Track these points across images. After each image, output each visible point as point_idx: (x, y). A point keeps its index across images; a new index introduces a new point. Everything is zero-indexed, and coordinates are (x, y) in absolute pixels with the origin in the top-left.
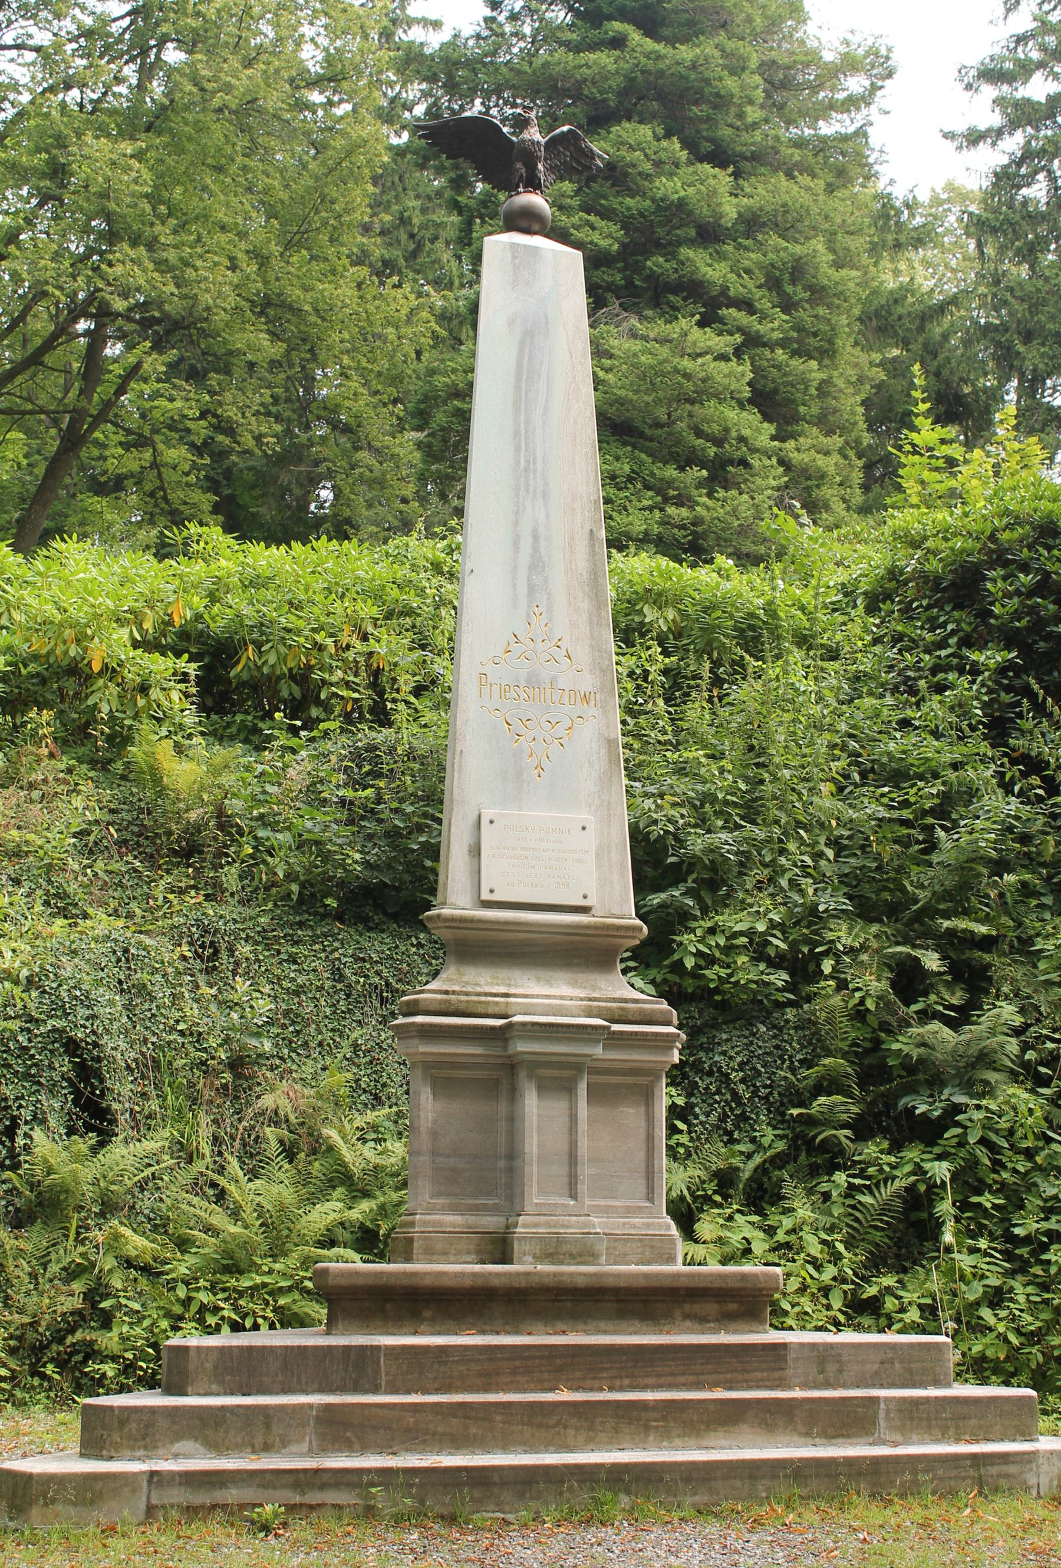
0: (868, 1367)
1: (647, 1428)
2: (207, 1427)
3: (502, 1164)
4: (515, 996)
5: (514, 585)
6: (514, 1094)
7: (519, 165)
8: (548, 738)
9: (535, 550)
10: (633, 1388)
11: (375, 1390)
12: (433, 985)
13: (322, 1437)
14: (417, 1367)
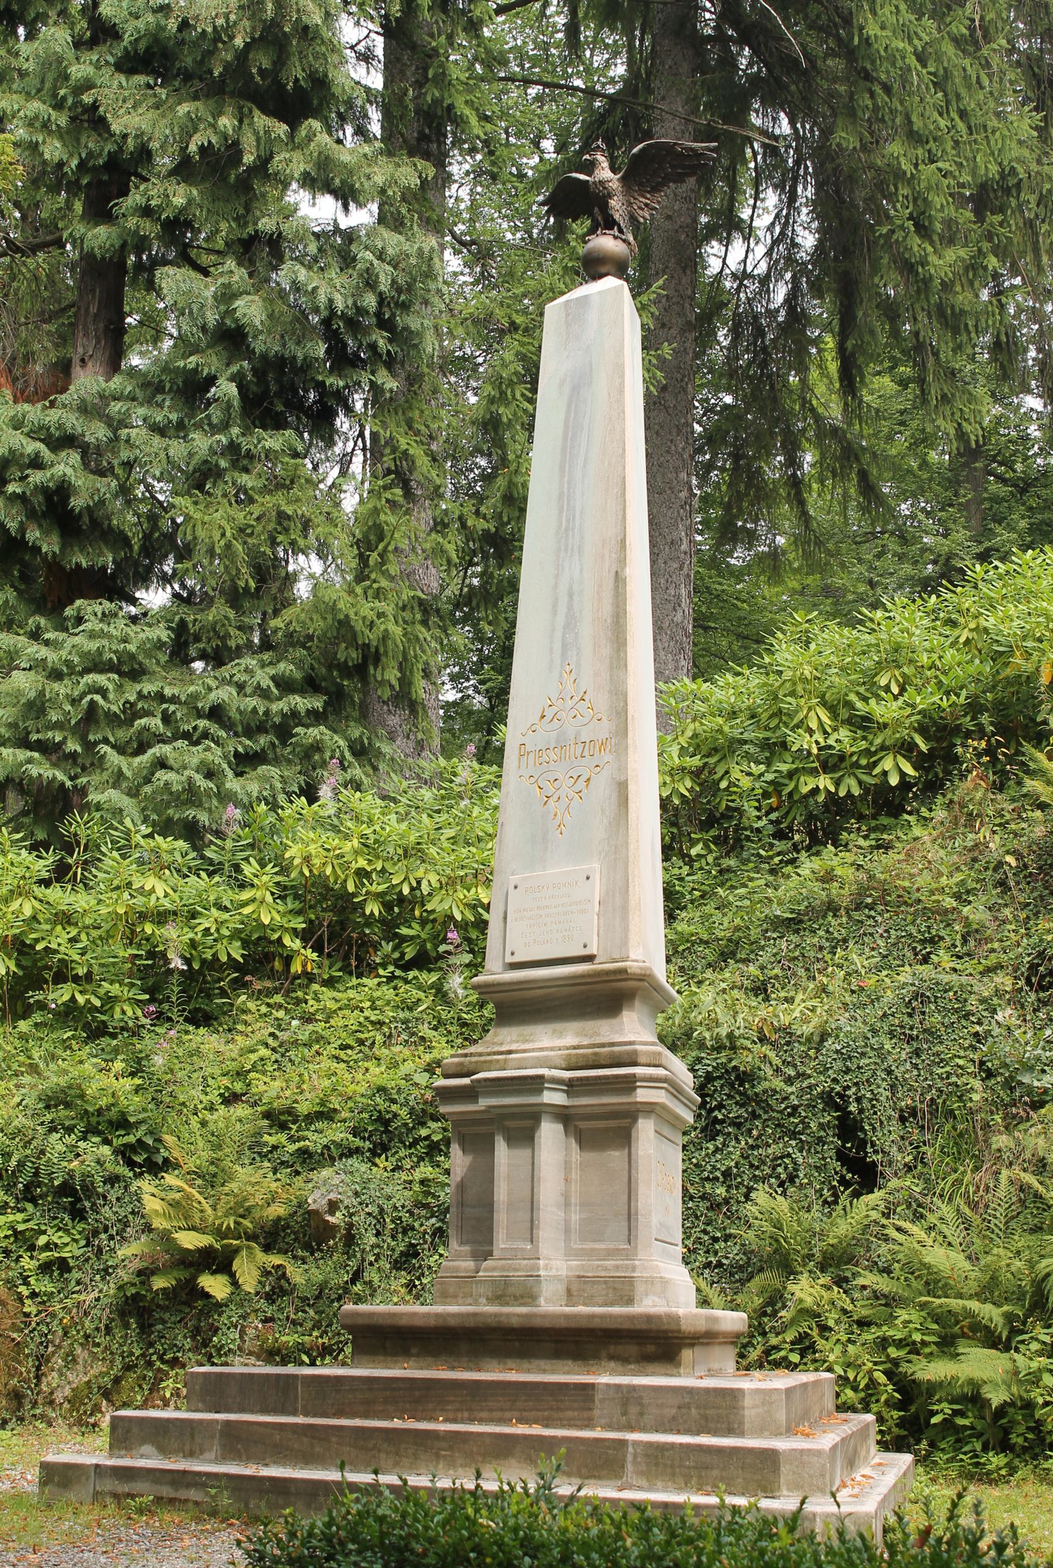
0: (667, 1411)
1: (438, 1456)
4: (510, 1052)
9: (570, 607)
10: (471, 1420)
11: (294, 1413)
13: (223, 1447)
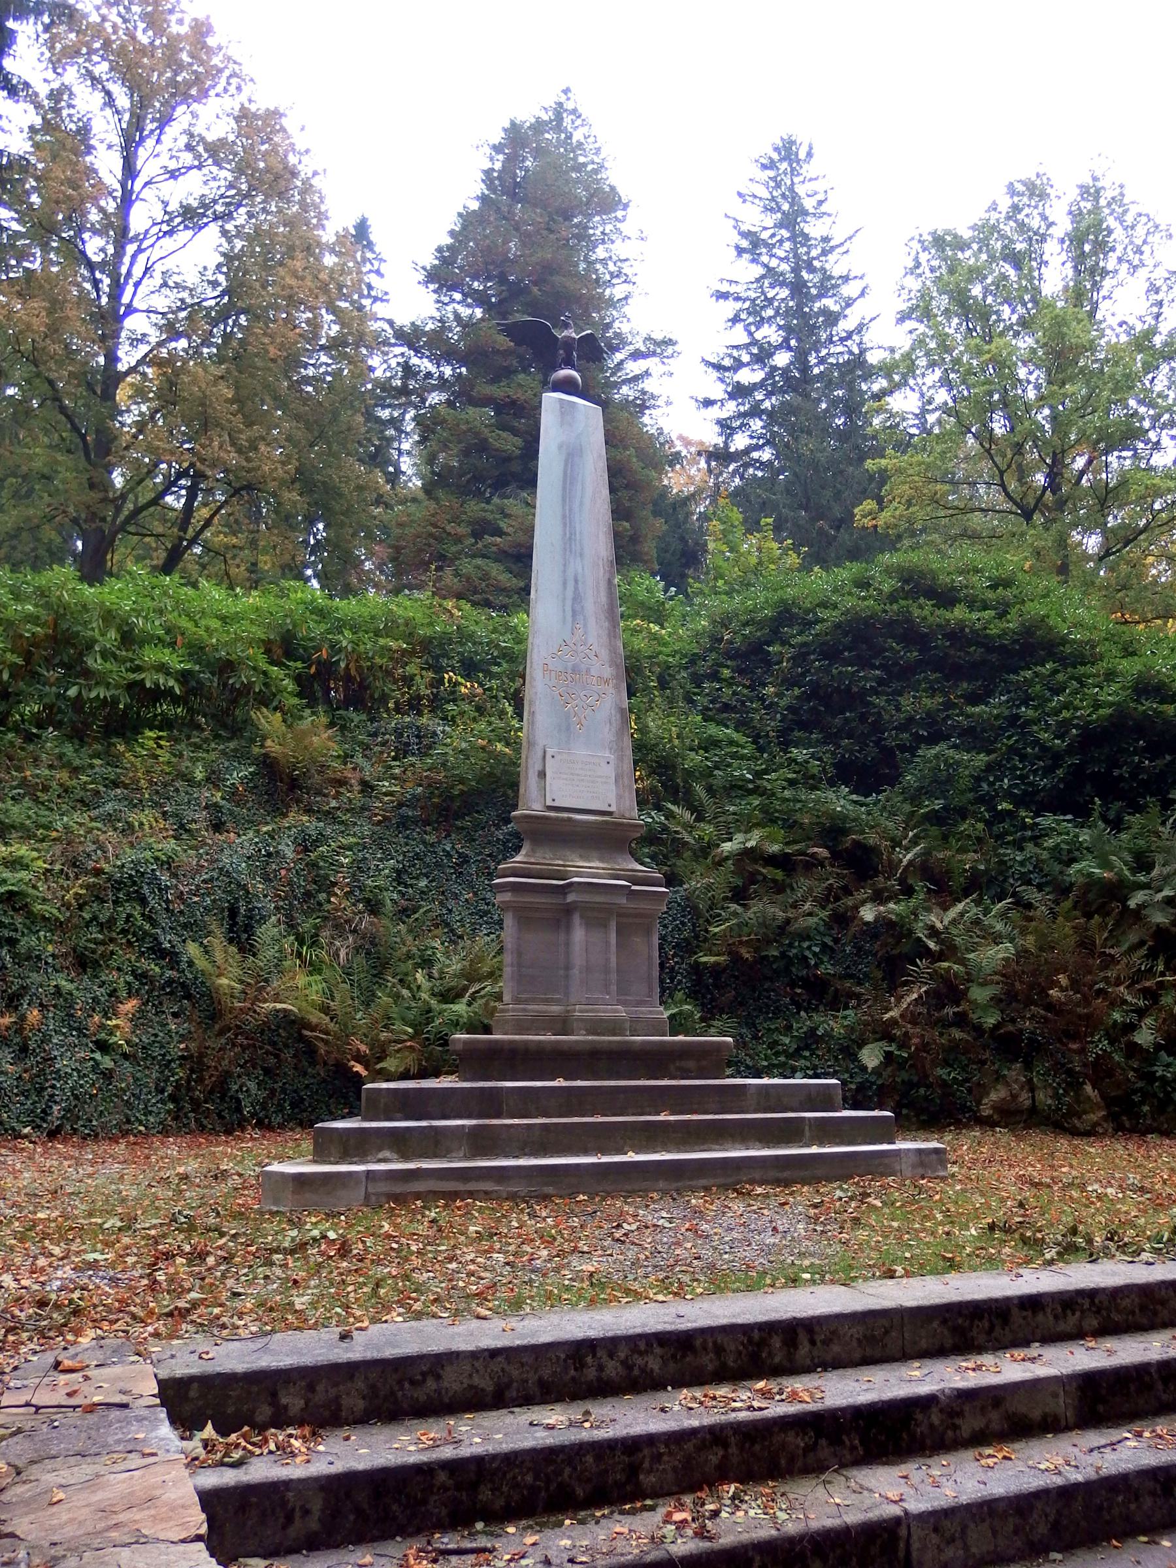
2: (401, 1143)
3: (562, 972)
6: (568, 928)
9: (576, 588)
12: (518, 859)
14: (528, 1102)
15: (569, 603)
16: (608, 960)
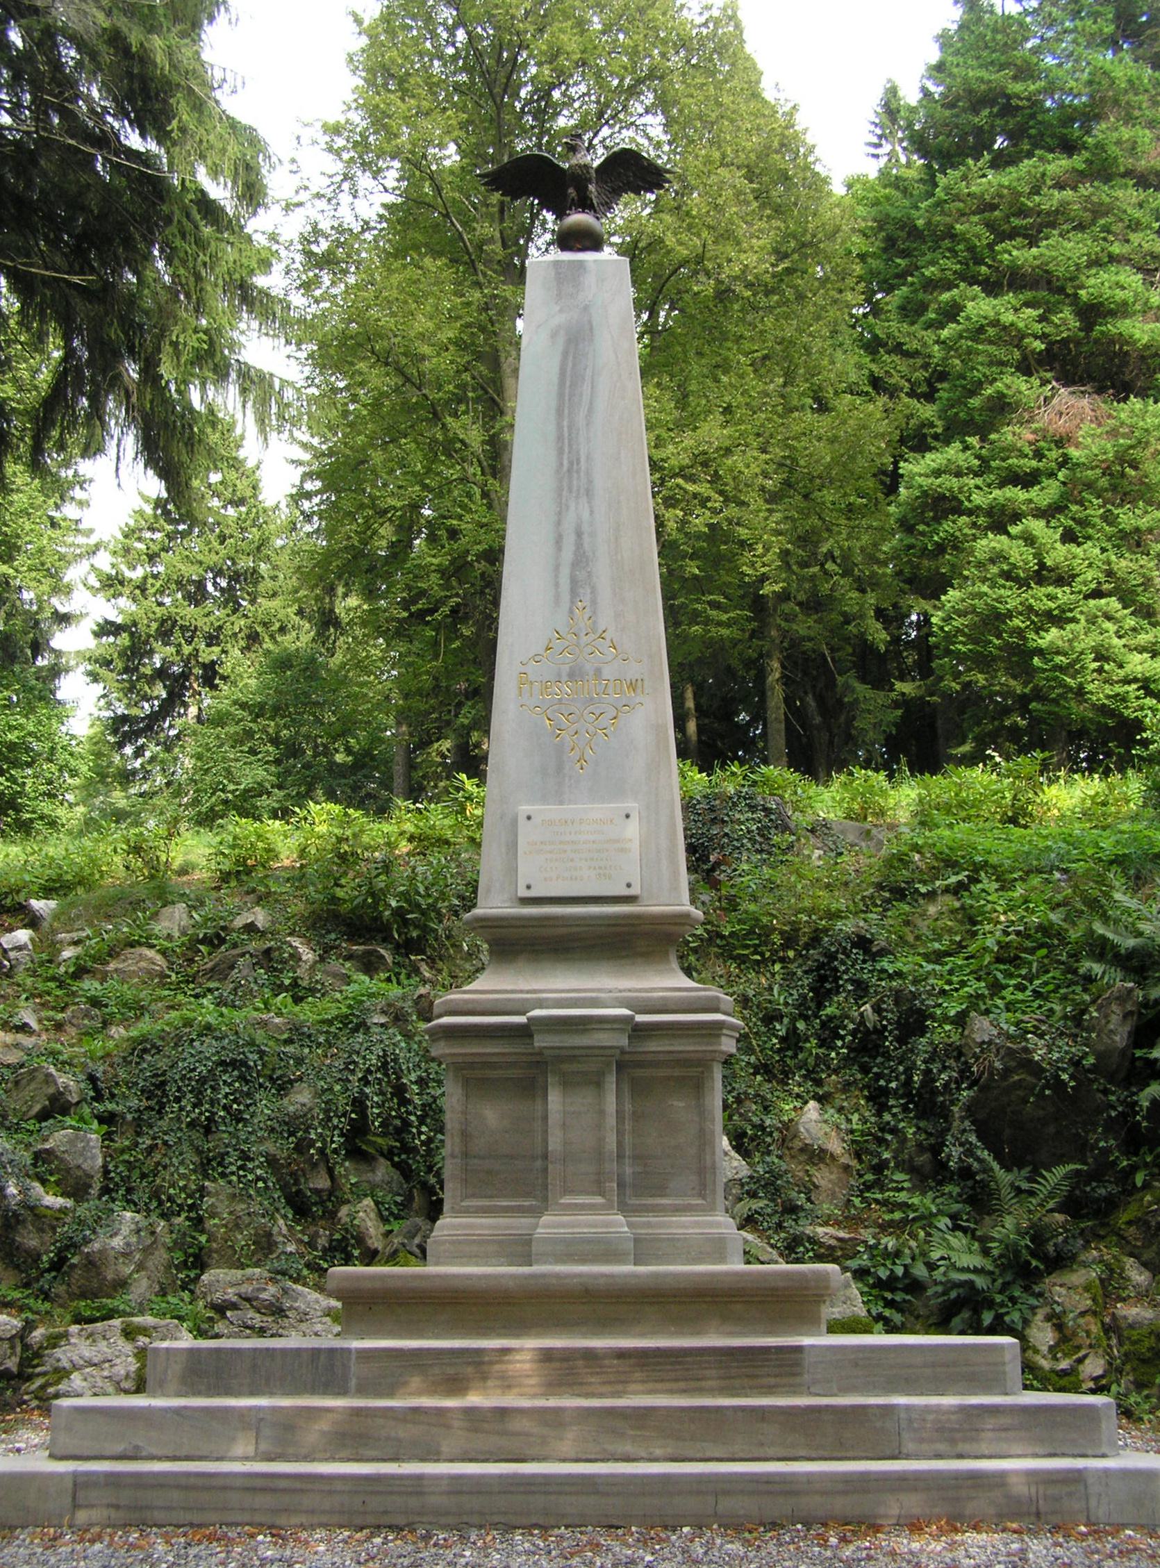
5: (557, 585)
7: (571, 190)
8: (591, 729)
9: (579, 545)
15: (565, 572)
16: (601, 1140)
